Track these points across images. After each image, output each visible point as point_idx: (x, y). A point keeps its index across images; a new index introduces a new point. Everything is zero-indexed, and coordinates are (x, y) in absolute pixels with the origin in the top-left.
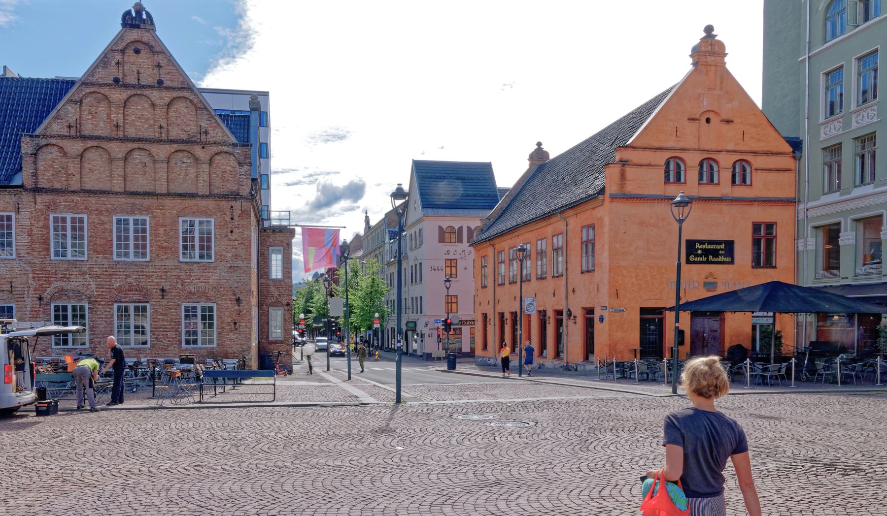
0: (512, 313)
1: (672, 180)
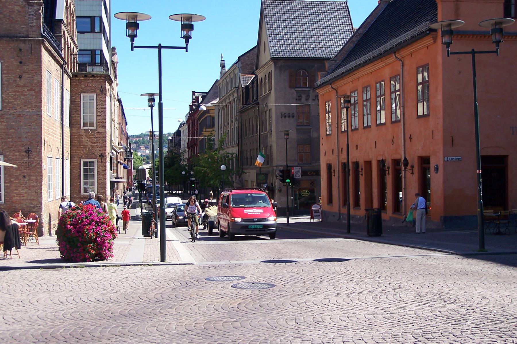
0: (379, 161)
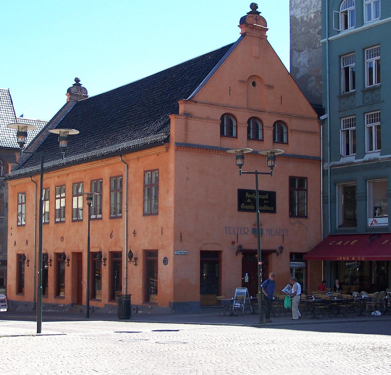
1: (225, 134)
